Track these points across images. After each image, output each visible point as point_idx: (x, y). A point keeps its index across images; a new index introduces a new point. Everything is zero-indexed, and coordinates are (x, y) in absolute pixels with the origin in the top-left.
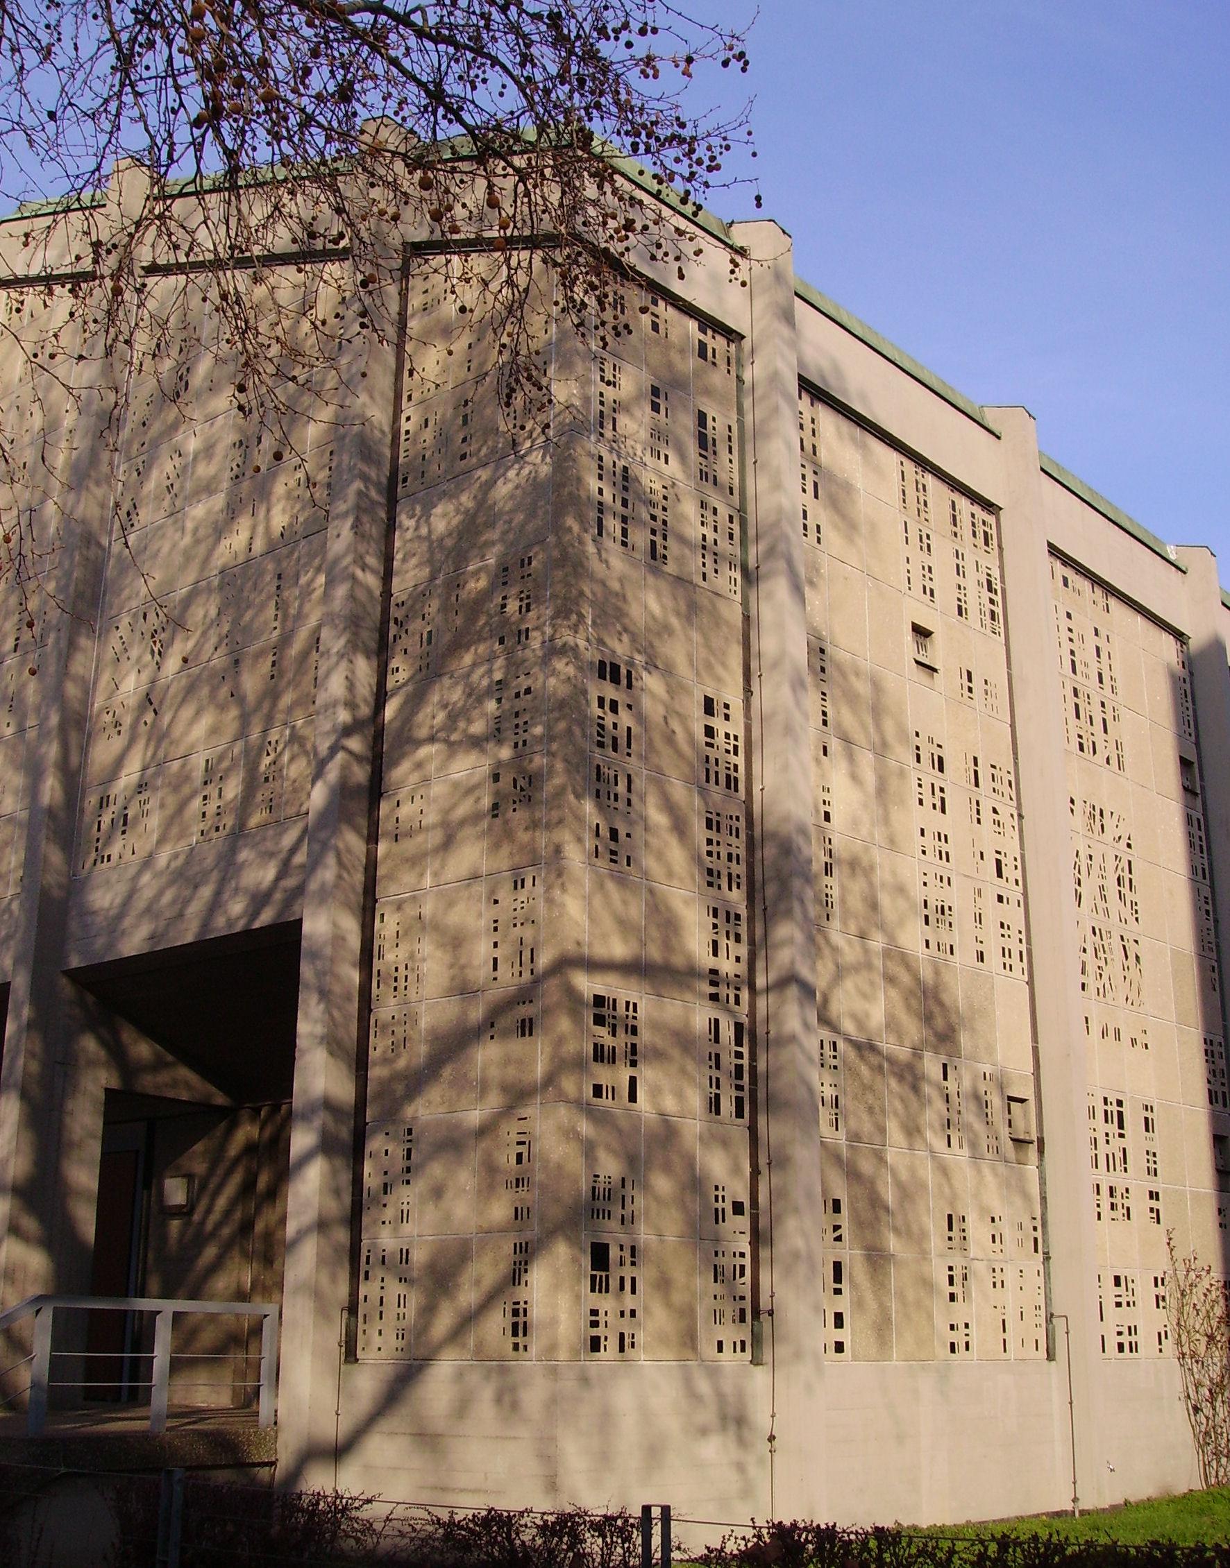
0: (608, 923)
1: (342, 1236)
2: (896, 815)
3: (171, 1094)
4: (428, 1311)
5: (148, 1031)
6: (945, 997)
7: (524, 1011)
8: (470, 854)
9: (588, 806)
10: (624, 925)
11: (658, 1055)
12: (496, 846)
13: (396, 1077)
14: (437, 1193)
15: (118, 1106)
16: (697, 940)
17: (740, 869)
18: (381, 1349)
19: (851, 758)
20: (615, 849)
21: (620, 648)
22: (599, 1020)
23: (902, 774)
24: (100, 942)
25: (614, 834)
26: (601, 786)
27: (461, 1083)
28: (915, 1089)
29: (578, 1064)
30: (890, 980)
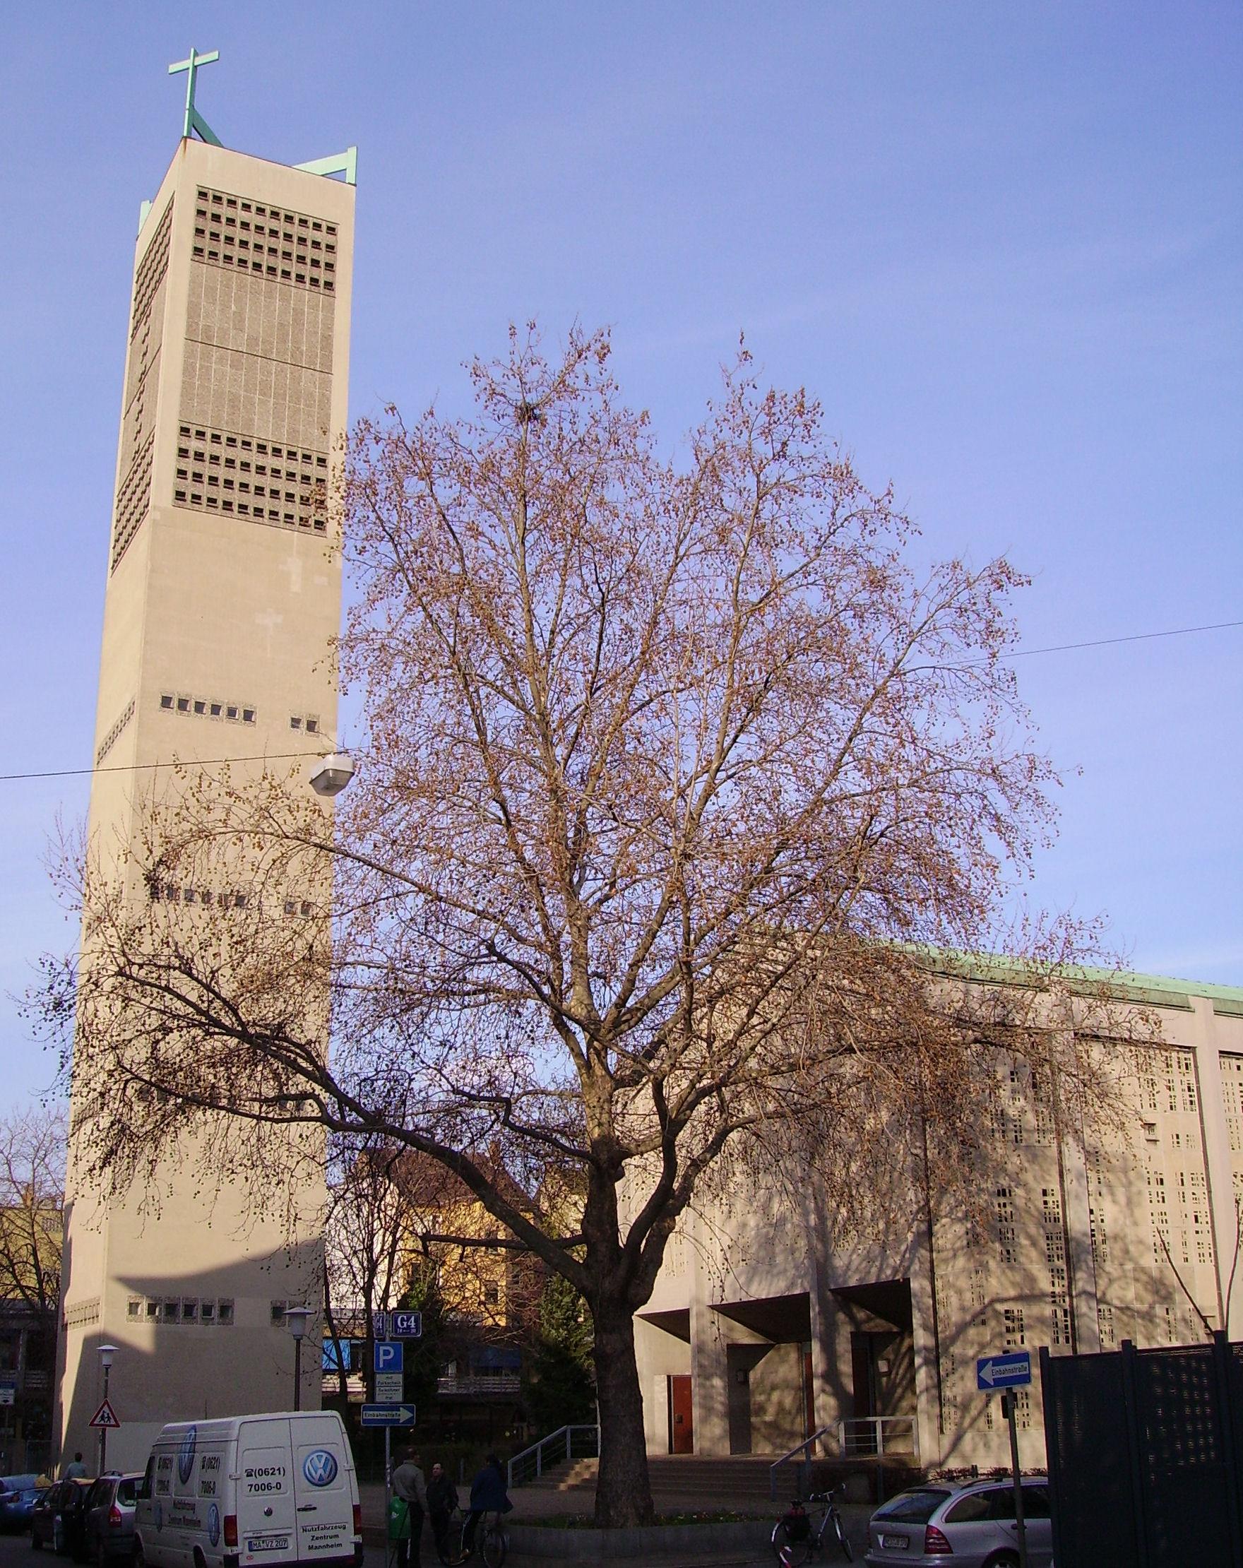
0: (1007, 1284)
1: (934, 1392)
2: (1137, 1212)
3: (876, 1330)
4: (963, 1417)
5: (863, 1306)
6: (1166, 1282)
7: (983, 1317)
8: (961, 1262)
9: (997, 1246)
10: (1013, 1284)
11: (1030, 1327)
12: (969, 1260)
13: (946, 1337)
14: (962, 1378)
15: (856, 1337)
16: (1044, 1282)
17: (1063, 1252)
18: (950, 1428)
19: (1112, 1194)
20: (1008, 1257)
21: (1004, 1182)
22: (1007, 1318)
23: (1140, 1193)
24: (841, 1280)
25: (1008, 1252)
26: (1001, 1237)
27: (966, 1342)
28: (1151, 1321)
29: (1001, 1335)
30: (1137, 1280)
